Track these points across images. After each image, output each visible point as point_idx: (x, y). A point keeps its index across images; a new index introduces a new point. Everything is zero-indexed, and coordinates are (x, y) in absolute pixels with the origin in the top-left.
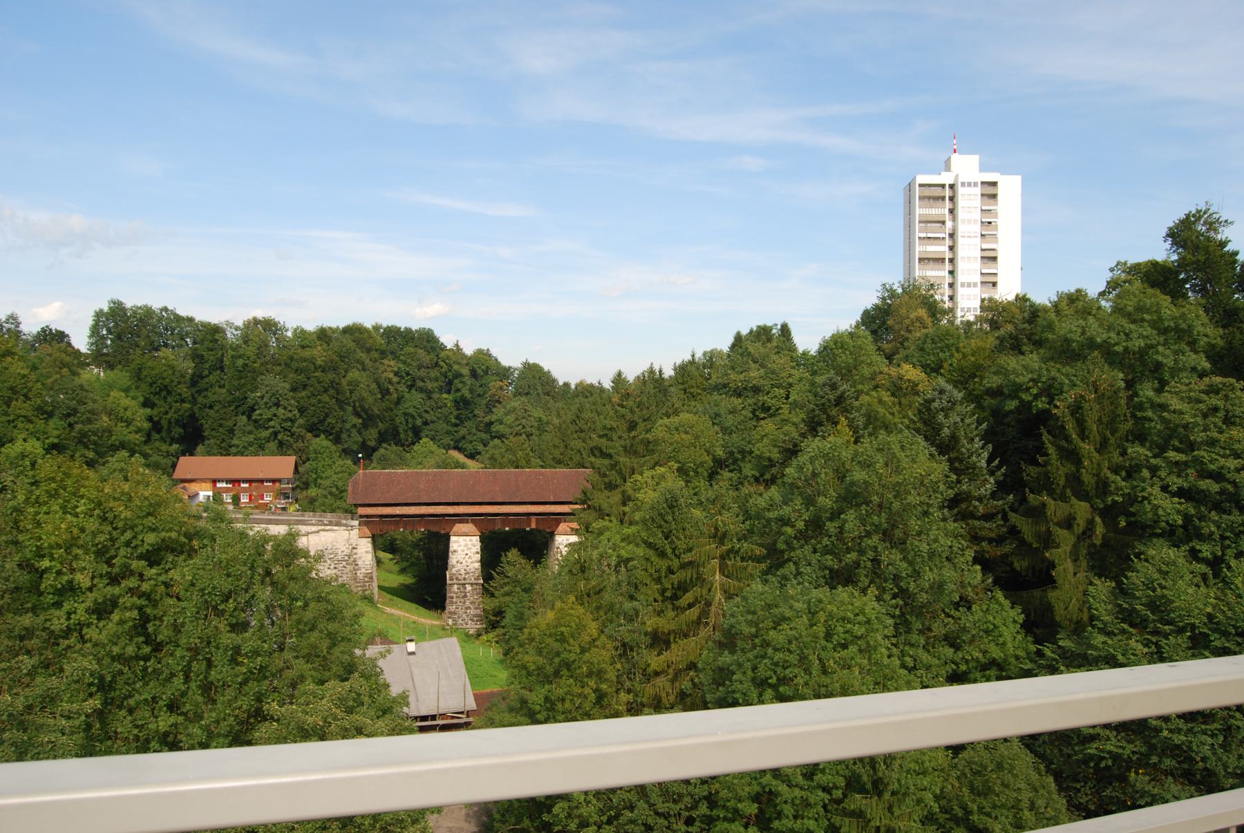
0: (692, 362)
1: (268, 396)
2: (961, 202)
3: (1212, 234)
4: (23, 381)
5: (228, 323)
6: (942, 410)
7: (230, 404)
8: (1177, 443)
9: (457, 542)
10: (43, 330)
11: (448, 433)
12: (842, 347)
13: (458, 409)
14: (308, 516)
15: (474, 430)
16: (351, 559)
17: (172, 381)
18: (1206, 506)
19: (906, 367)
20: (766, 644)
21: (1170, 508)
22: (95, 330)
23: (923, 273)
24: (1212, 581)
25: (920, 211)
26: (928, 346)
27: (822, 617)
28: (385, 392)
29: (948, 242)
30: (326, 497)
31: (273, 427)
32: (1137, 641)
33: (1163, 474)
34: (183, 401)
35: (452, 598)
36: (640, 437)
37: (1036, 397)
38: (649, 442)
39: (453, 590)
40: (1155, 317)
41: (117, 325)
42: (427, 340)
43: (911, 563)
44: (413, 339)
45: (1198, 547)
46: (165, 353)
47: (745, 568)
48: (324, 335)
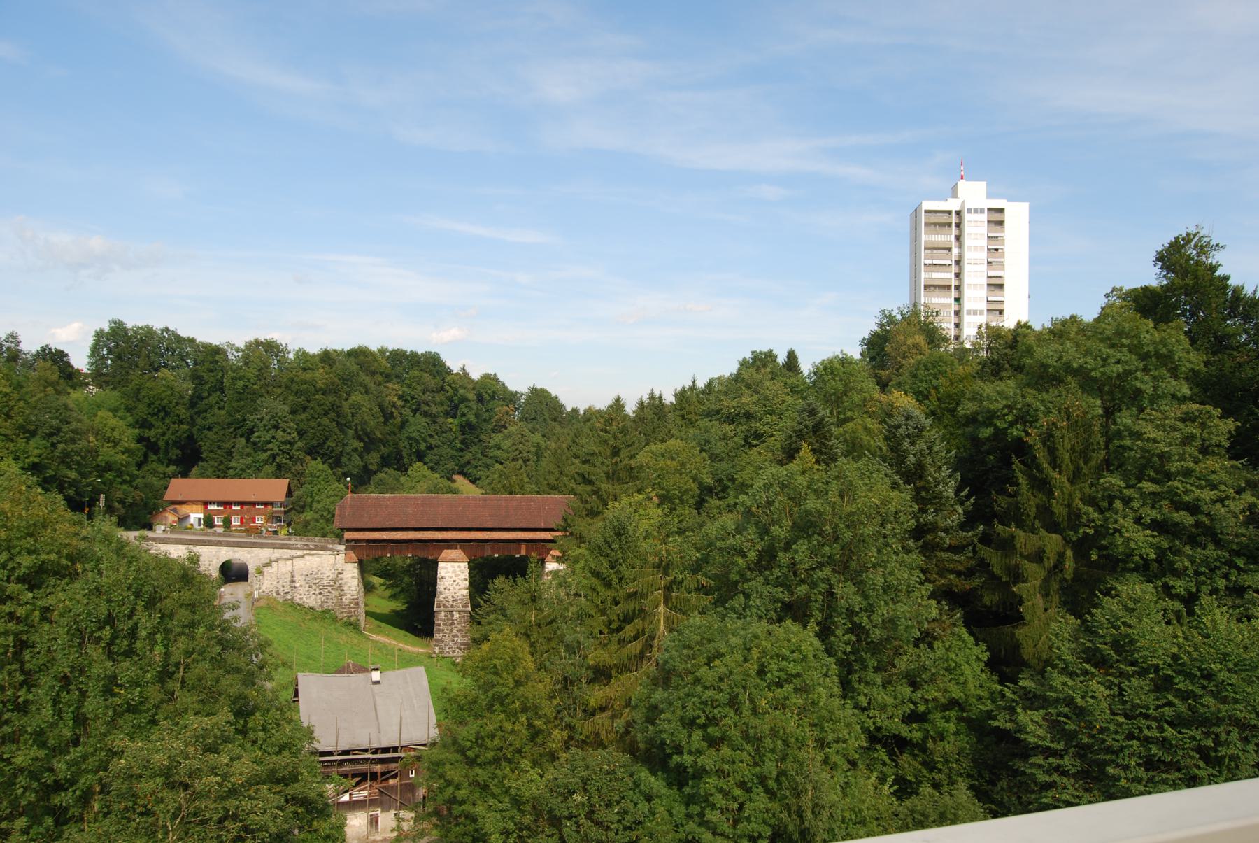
0: (693, 388)
1: (267, 418)
2: (967, 229)
3: (1203, 258)
4: (5, 399)
5: (229, 344)
6: (908, 436)
7: (229, 425)
8: (1152, 473)
9: (446, 568)
10: (43, 349)
11: (453, 457)
12: (832, 373)
13: (464, 434)
14: (295, 541)
15: (479, 456)
16: (336, 584)
17: (170, 402)
18: (1181, 539)
19: (897, 394)
20: (697, 681)
21: (1142, 541)
22: (95, 350)
23: (928, 300)
24: (1186, 619)
25: (925, 237)
26: (921, 372)
27: (755, 653)
28: (388, 416)
29: (954, 269)
30: (317, 521)
31: (272, 450)
32: (1099, 683)
33: (1136, 505)
34: (181, 422)
35: (439, 625)
36: (624, 463)
37: (1011, 424)
38: (632, 468)
39: (441, 617)
40: (1135, 342)
41: (117, 345)
42: (433, 364)
43: (866, 597)
44: (419, 362)
45: (1171, 583)
46: (164, 373)
47: (689, 600)
48: (327, 358)
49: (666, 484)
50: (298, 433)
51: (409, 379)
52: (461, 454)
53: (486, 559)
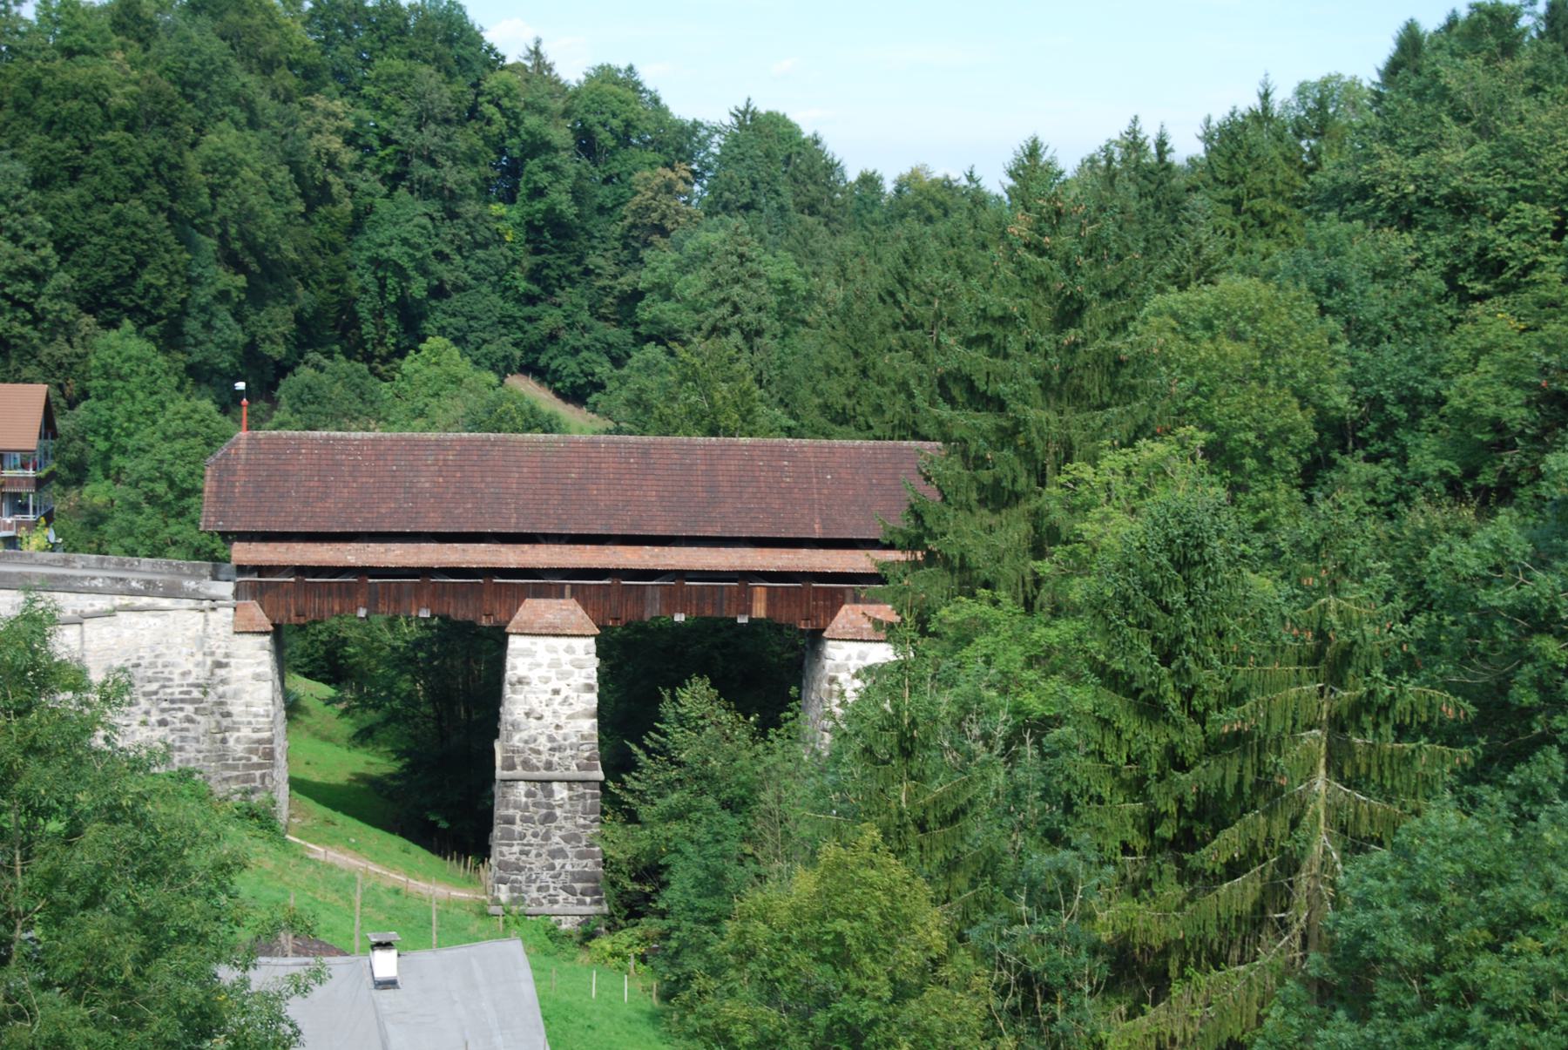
0: (1262, 117)
11: (506, 322)
13: (537, 251)
15: (584, 317)
28: (316, 196)
30: (135, 508)
36: (1094, 347)
38: (1119, 363)
44: (402, 31)
47: (1408, 760)
49: (1217, 413)
50: (58, 247)
51: (375, 82)
52: (529, 310)
53: (642, 628)
